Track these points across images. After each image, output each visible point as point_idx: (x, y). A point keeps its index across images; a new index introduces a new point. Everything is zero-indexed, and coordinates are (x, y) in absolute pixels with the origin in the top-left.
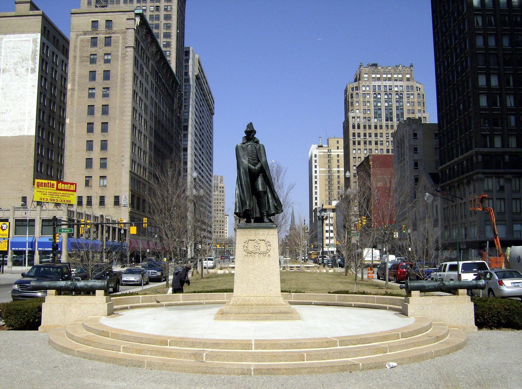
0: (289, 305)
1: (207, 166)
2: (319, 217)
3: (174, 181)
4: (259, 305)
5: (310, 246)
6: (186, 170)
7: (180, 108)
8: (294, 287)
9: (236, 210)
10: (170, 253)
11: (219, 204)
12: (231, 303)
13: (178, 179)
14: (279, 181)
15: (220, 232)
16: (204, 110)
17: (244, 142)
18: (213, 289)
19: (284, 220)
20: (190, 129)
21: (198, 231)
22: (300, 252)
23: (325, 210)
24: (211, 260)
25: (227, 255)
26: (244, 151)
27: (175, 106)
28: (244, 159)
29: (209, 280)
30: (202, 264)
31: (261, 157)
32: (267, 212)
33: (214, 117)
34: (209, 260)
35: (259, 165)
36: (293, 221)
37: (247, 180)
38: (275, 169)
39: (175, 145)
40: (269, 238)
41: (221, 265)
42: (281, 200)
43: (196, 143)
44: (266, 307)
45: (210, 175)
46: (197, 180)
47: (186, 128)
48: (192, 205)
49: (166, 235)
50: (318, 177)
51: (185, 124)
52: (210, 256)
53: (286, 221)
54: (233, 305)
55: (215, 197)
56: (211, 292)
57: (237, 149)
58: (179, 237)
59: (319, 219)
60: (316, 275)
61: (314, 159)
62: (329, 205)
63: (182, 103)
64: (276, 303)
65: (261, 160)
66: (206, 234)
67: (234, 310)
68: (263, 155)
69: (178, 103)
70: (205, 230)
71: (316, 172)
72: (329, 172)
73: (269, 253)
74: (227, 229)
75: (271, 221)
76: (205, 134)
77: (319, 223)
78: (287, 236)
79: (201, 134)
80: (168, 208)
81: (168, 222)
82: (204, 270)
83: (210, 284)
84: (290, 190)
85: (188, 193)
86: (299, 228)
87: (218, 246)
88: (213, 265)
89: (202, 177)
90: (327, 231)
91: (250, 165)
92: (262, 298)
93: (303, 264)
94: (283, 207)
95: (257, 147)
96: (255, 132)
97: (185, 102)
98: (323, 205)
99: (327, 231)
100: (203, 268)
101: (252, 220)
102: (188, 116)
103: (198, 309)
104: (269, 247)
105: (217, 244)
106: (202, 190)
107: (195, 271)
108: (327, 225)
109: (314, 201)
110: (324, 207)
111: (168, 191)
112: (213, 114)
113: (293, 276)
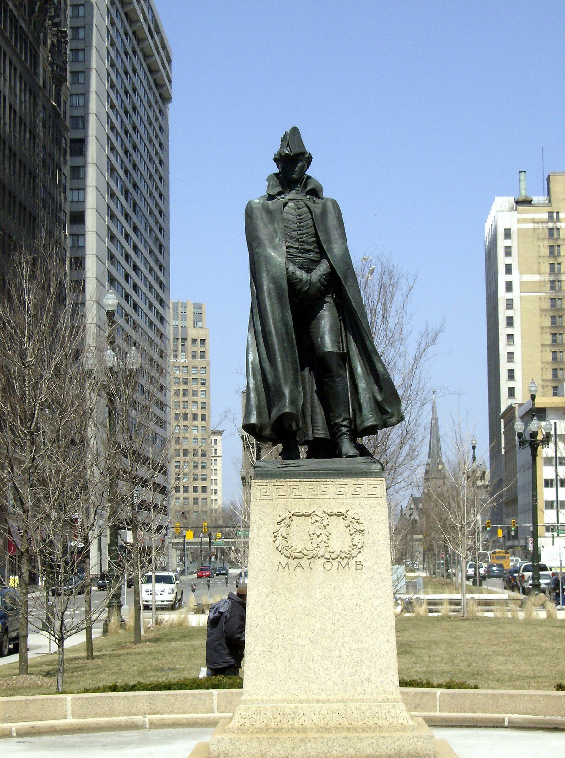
0: (426, 731)
1: (151, 270)
2: (520, 435)
3: (45, 322)
4: (326, 729)
5: (494, 532)
6: (79, 285)
7: (59, 81)
8: (441, 668)
9: (247, 415)
10: (31, 561)
11: (190, 398)
12: (235, 723)
13: (55, 318)
14: (391, 321)
15: (195, 489)
16: (138, 86)
17: (274, 192)
18: (173, 677)
19: (406, 448)
20: (94, 151)
21: (123, 487)
22: (461, 552)
23: (540, 413)
24: (167, 580)
25: (218, 565)
26: (272, 222)
27: (43, 73)
28: (275, 248)
29: (160, 647)
30: (137, 594)
31: (329, 242)
32: (352, 421)
33: (172, 109)
34: (160, 579)
35: (322, 268)
36: (435, 452)
37: (284, 320)
38: (374, 279)
39: (44, 201)
40: (358, 508)
41: (197, 597)
42: (397, 381)
43: (112, 195)
44: (351, 735)
45: (161, 302)
46: (120, 320)
47: (79, 147)
48: (104, 401)
49: (19, 499)
50: (517, 304)
51: (77, 135)
52: (164, 569)
53: (412, 449)
54: (242, 729)
55: (179, 374)
56: (168, 687)
57: (249, 214)
58: (61, 508)
59: (522, 443)
60: (514, 629)
61: (502, 243)
62: (555, 394)
63: (65, 63)
64: (386, 724)
65: (331, 250)
66: (148, 495)
67: (244, 749)
68: (335, 234)
69: (51, 64)
70: (145, 484)
71: (509, 286)
72: (553, 288)
73: (360, 558)
74: (219, 487)
75: (363, 451)
76: (141, 166)
77: (523, 455)
78: (416, 501)
79: (130, 168)
80: (23, 411)
81: (25, 456)
82: (146, 616)
83: (165, 662)
84: (427, 347)
85: (89, 361)
86: (455, 474)
87: (190, 536)
88: (171, 597)
89: (135, 306)
90: (548, 483)
91: (292, 268)
92: (336, 706)
93: (471, 592)
94: (403, 405)
95: (317, 209)
96: (309, 160)
97: (75, 60)
98: (533, 397)
99: (548, 483)
100: (142, 607)
101: (303, 450)
102: (86, 106)
103: (127, 744)
104: (358, 537)
105: (186, 527)
106: (133, 352)
107: (114, 620)
108: (548, 461)
109: (504, 384)
110: (540, 402)
111: (23, 356)
112: (166, 99)
113: (437, 633)
